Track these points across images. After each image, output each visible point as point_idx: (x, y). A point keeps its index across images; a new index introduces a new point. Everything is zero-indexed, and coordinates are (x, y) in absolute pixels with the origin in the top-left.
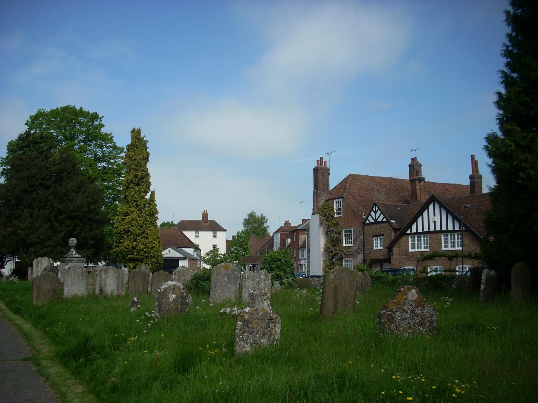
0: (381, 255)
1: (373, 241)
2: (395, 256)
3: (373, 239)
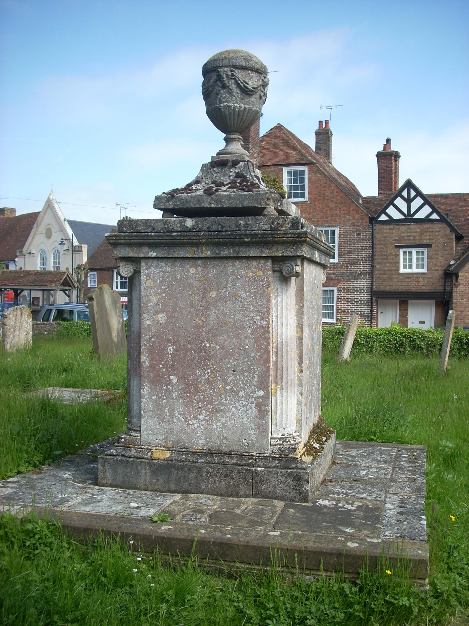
0: (421, 284)
1: (399, 255)
2: (461, 288)
3: (399, 252)
